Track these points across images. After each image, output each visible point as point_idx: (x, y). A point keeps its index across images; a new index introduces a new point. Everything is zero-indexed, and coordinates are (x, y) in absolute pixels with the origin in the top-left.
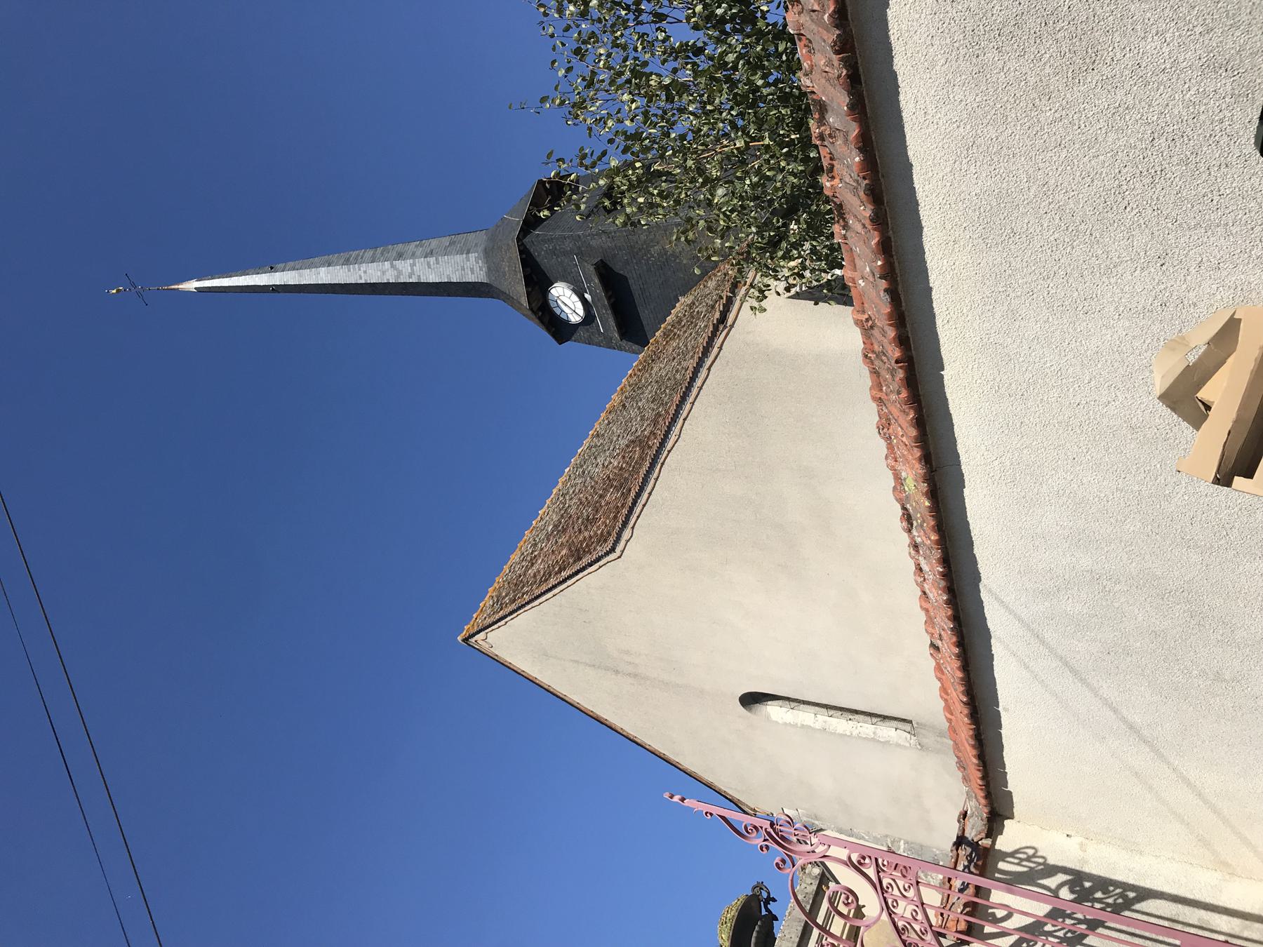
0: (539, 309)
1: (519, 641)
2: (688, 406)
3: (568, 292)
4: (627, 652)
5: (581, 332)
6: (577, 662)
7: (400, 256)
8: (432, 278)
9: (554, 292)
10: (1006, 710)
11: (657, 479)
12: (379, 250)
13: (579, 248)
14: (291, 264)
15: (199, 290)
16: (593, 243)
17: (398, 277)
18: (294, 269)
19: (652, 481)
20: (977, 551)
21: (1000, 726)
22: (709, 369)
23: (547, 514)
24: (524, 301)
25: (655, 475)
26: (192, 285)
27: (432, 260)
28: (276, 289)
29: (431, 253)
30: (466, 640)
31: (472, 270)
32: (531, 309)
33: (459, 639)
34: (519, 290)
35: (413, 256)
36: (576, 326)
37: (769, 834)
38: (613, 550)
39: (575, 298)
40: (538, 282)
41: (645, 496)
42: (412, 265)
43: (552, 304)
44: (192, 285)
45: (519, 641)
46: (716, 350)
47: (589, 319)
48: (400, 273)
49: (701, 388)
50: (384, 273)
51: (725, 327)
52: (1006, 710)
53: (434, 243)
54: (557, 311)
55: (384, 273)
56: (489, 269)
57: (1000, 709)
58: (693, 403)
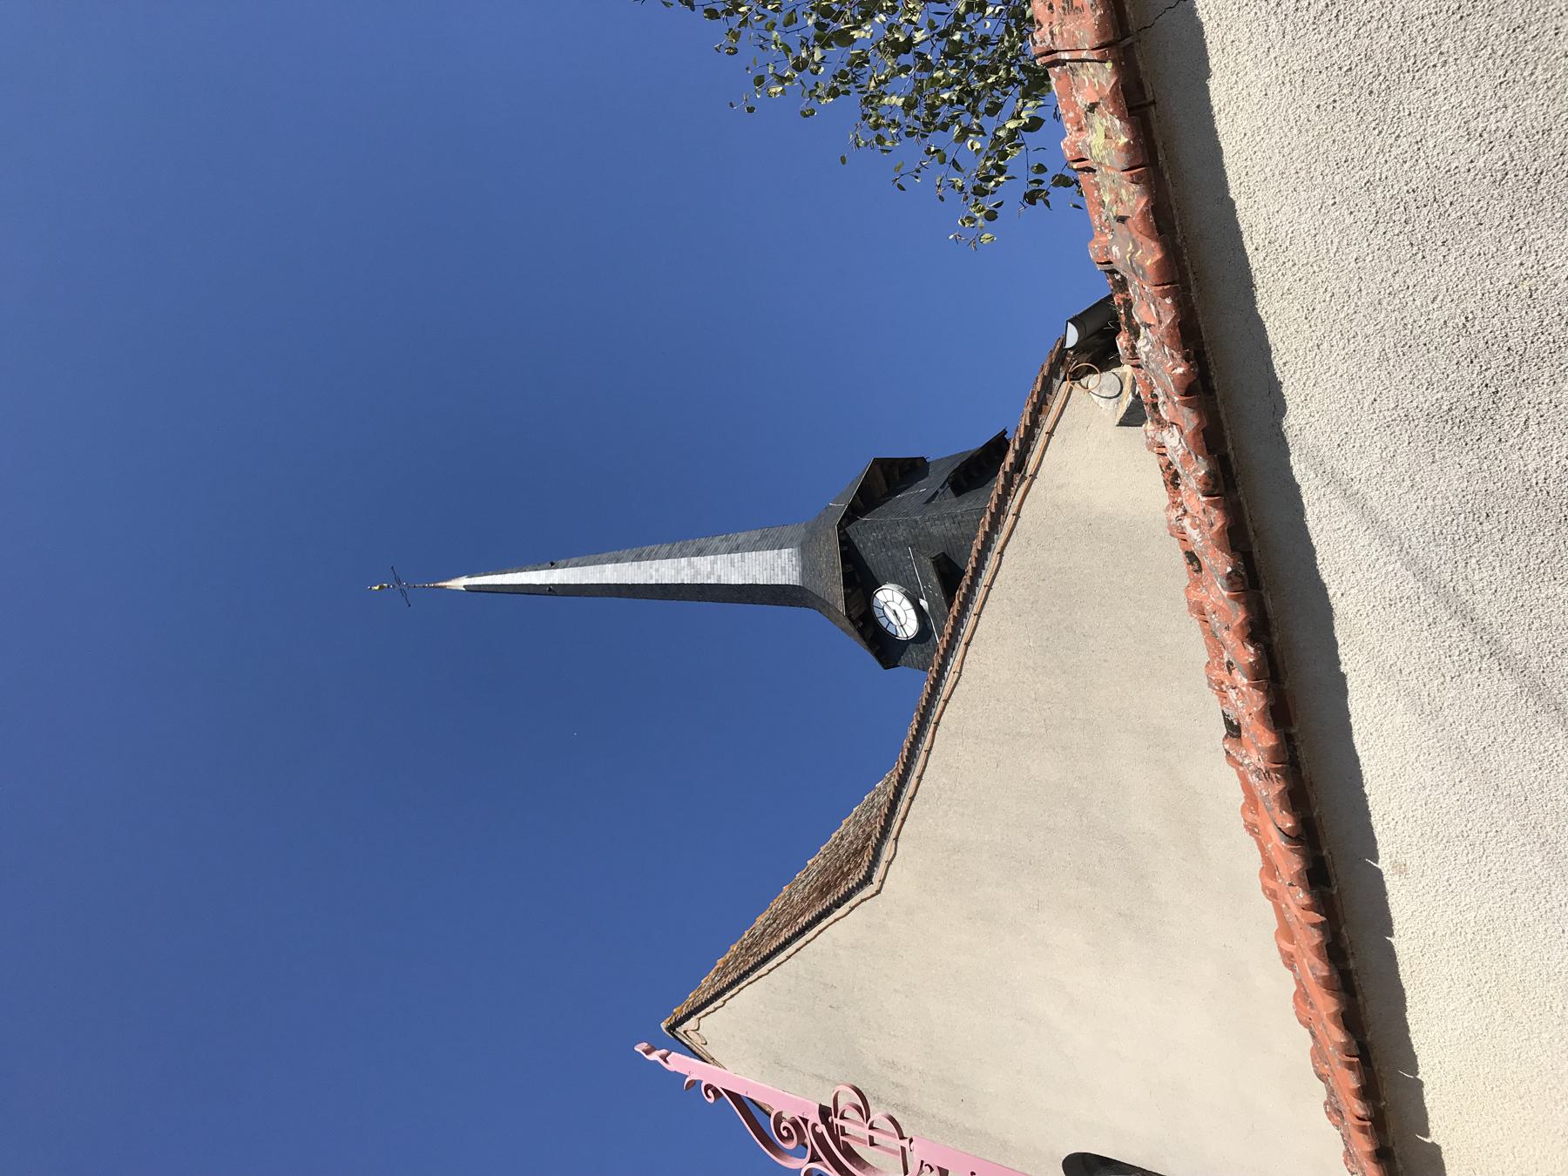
0: (861, 618)
1: (749, 1043)
2: (971, 620)
3: (899, 597)
4: (892, 1065)
5: (913, 653)
6: (820, 1077)
7: (700, 552)
8: (735, 579)
9: (880, 596)
10: (1401, 869)
11: (928, 752)
12: (677, 545)
13: (916, 537)
14: (575, 560)
15: (470, 589)
16: (934, 530)
17: (695, 576)
18: (577, 565)
19: (923, 756)
20: (1266, 306)
21: (1387, 926)
22: (1001, 553)
23: (815, 863)
24: (841, 606)
25: (926, 745)
26: (460, 583)
27: (737, 556)
28: (553, 590)
29: (737, 549)
30: (672, 1028)
31: (783, 569)
32: (849, 616)
33: (663, 1026)
34: (836, 592)
35: (716, 552)
36: (908, 642)
37: (819, 1138)
38: (868, 879)
39: (907, 604)
40: (861, 582)
41: (913, 780)
42: (714, 562)
43: (878, 613)
44: (460, 583)
45: (749, 1043)
46: (1010, 519)
47: (924, 634)
48: (697, 573)
49: (990, 588)
50: (678, 572)
51: (1023, 478)
52: (1401, 869)
53: (742, 537)
54: (884, 623)
55: (678, 572)
56: (804, 568)
57: (1383, 864)
58: (979, 615)
